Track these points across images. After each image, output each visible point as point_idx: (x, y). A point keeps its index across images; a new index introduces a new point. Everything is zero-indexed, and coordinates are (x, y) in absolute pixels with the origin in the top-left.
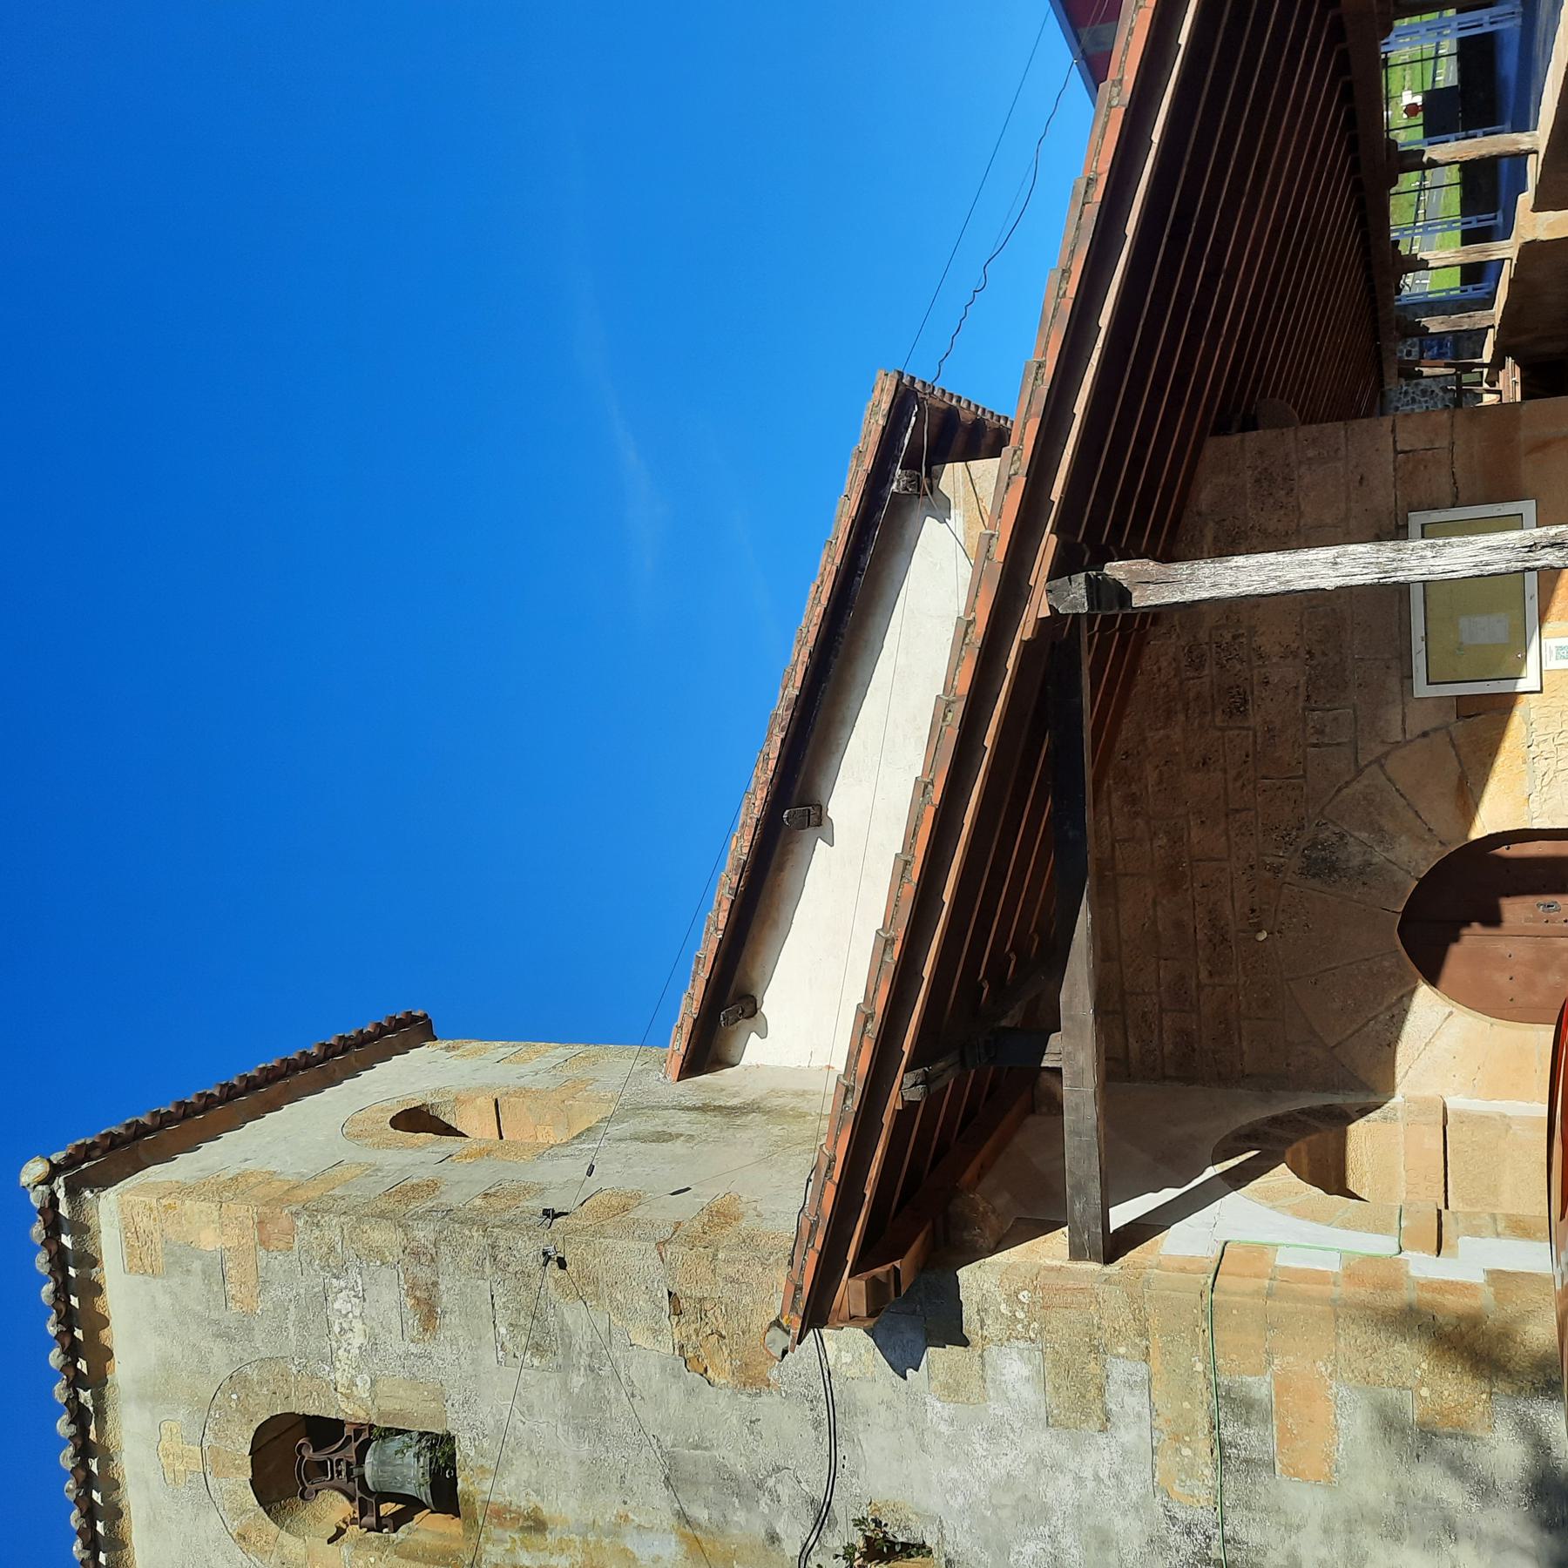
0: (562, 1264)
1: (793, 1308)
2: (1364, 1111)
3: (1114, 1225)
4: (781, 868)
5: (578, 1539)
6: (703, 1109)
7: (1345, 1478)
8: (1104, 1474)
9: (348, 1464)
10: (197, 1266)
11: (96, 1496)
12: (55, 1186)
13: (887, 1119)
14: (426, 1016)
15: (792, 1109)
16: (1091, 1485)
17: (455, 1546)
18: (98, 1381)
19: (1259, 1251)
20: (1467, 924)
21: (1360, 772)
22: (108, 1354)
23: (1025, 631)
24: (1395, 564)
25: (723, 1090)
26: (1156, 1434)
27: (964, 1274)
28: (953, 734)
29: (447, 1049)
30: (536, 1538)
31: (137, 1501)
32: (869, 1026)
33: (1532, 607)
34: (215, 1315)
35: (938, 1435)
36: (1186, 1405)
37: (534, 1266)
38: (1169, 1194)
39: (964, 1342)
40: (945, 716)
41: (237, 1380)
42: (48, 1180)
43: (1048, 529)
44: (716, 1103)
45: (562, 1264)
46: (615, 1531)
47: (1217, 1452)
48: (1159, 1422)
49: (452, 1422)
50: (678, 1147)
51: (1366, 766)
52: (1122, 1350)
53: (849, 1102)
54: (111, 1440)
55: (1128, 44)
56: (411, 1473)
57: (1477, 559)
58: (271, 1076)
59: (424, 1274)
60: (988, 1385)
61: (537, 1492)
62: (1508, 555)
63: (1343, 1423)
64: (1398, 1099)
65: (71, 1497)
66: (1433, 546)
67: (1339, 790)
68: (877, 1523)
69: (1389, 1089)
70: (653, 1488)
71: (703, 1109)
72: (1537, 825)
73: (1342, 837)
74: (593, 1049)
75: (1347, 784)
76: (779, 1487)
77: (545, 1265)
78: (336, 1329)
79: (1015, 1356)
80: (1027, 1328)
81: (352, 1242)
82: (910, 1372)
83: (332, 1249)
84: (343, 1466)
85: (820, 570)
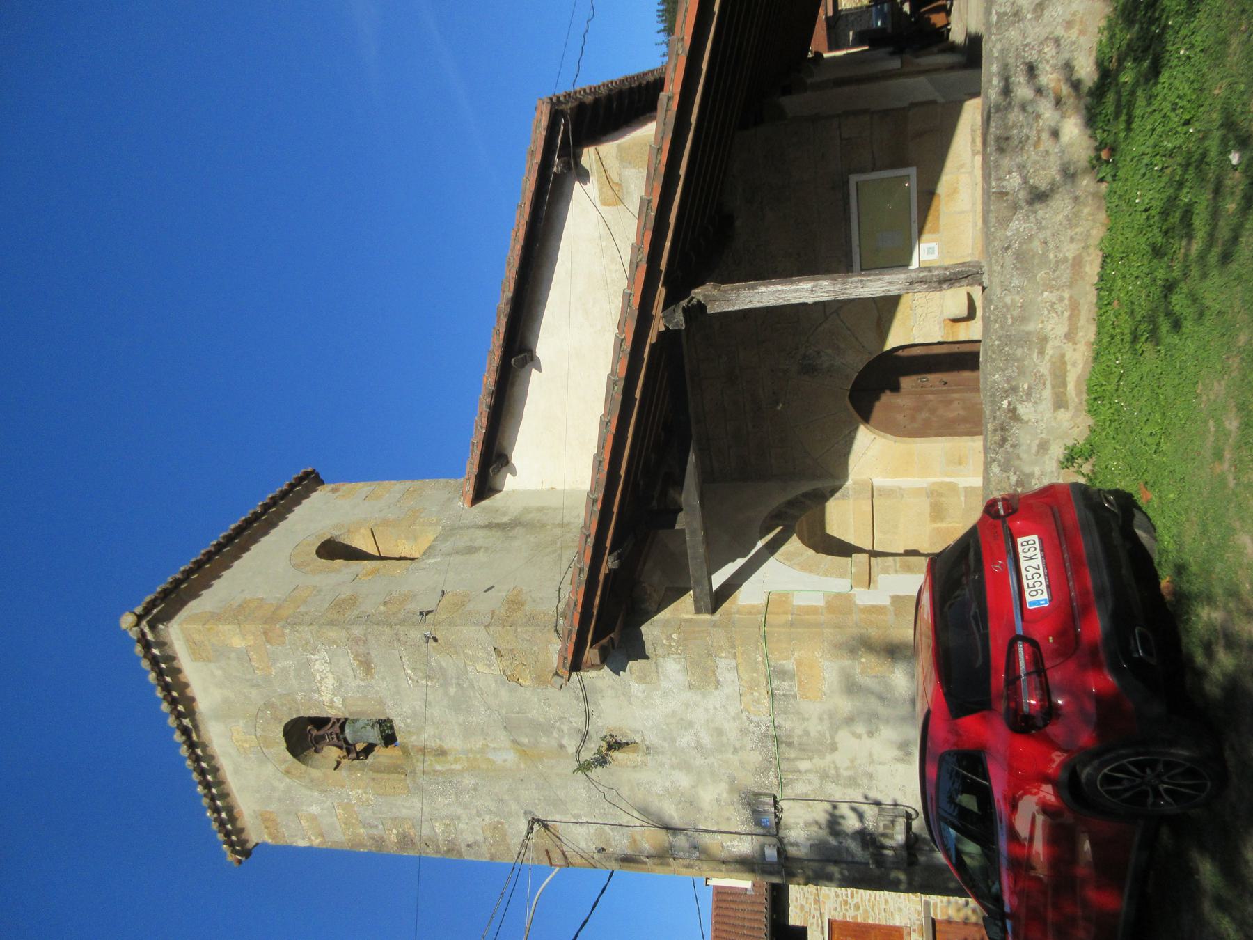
0: (435, 639)
1: (564, 666)
2: (833, 491)
3: (715, 586)
4: (513, 385)
5: (464, 757)
6: (489, 526)
8: (718, 706)
9: (337, 734)
10: (233, 655)
11: (209, 778)
12: (142, 626)
13: (601, 578)
14: (314, 470)
15: (538, 521)
16: (712, 711)
17: (399, 762)
18: (191, 713)
19: (784, 597)
21: (827, 318)
22: (193, 700)
23: (652, 338)
24: (843, 291)
25: (497, 511)
26: (741, 688)
28: (619, 398)
29: (335, 490)
30: (442, 758)
31: (227, 765)
32: (589, 540)
33: (915, 227)
34: (249, 677)
35: (637, 698)
36: (755, 675)
37: (422, 642)
38: (740, 562)
39: (647, 658)
40: (614, 388)
43: (660, 286)
44: (496, 521)
45: (435, 639)
46: (483, 750)
47: (770, 693)
48: (743, 683)
49: (391, 712)
50: (481, 556)
51: (831, 314)
52: (723, 655)
53: (582, 575)
54: (205, 738)
55: (685, 17)
56: (373, 735)
57: (884, 289)
58: (239, 531)
59: (361, 649)
60: (660, 675)
61: (440, 739)
62: (898, 286)
63: (827, 676)
64: (849, 483)
65: (191, 768)
66: (861, 281)
67: (817, 328)
68: (612, 736)
69: (844, 475)
70: (498, 732)
71: (489, 526)
72: (916, 342)
73: (818, 353)
74: (417, 483)
76: (562, 726)
77: (427, 642)
79: (672, 661)
81: (318, 637)
82: (621, 673)
84: (334, 736)
85: (516, 222)
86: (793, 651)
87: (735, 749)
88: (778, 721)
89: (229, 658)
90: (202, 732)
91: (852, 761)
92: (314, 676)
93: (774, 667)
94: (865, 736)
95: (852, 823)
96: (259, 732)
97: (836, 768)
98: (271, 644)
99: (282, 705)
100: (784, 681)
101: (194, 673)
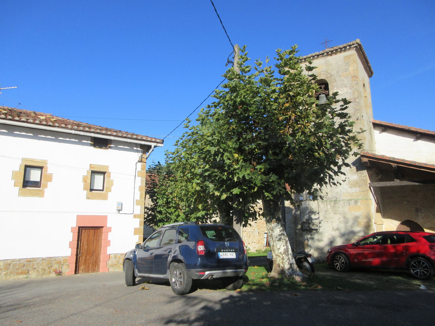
7: (160, 205)
10: (347, 67)
20: (410, 228)
27: (366, 171)
41: (331, 76)
42: (357, 43)
64: (383, 219)
75: (431, 213)
78: (342, 89)
80: (360, 178)
83: (353, 87)
86: (363, 205)
87: (332, 191)
88: (341, 201)
89: (346, 66)
90: (321, 58)
91: (331, 218)
92: (342, 88)
93: (358, 201)
94: (339, 221)
95: (313, 216)
96: (322, 73)
97: (329, 214)
98: (351, 78)
99: (332, 79)
100: (354, 203)
101: (340, 56)
